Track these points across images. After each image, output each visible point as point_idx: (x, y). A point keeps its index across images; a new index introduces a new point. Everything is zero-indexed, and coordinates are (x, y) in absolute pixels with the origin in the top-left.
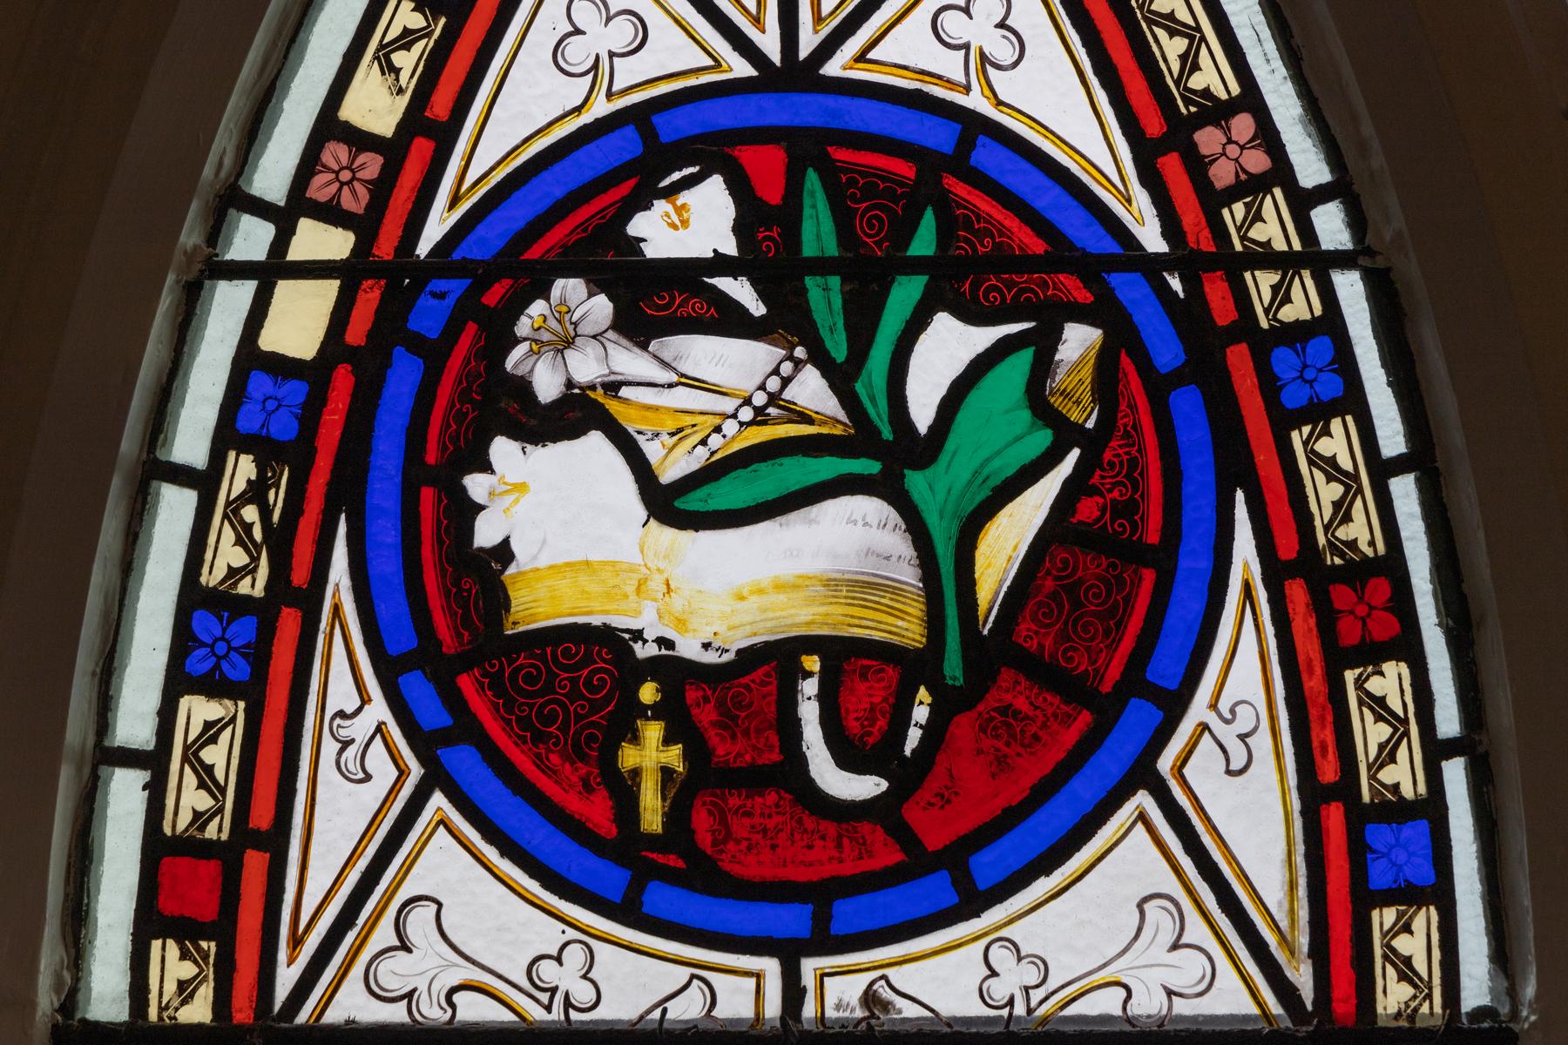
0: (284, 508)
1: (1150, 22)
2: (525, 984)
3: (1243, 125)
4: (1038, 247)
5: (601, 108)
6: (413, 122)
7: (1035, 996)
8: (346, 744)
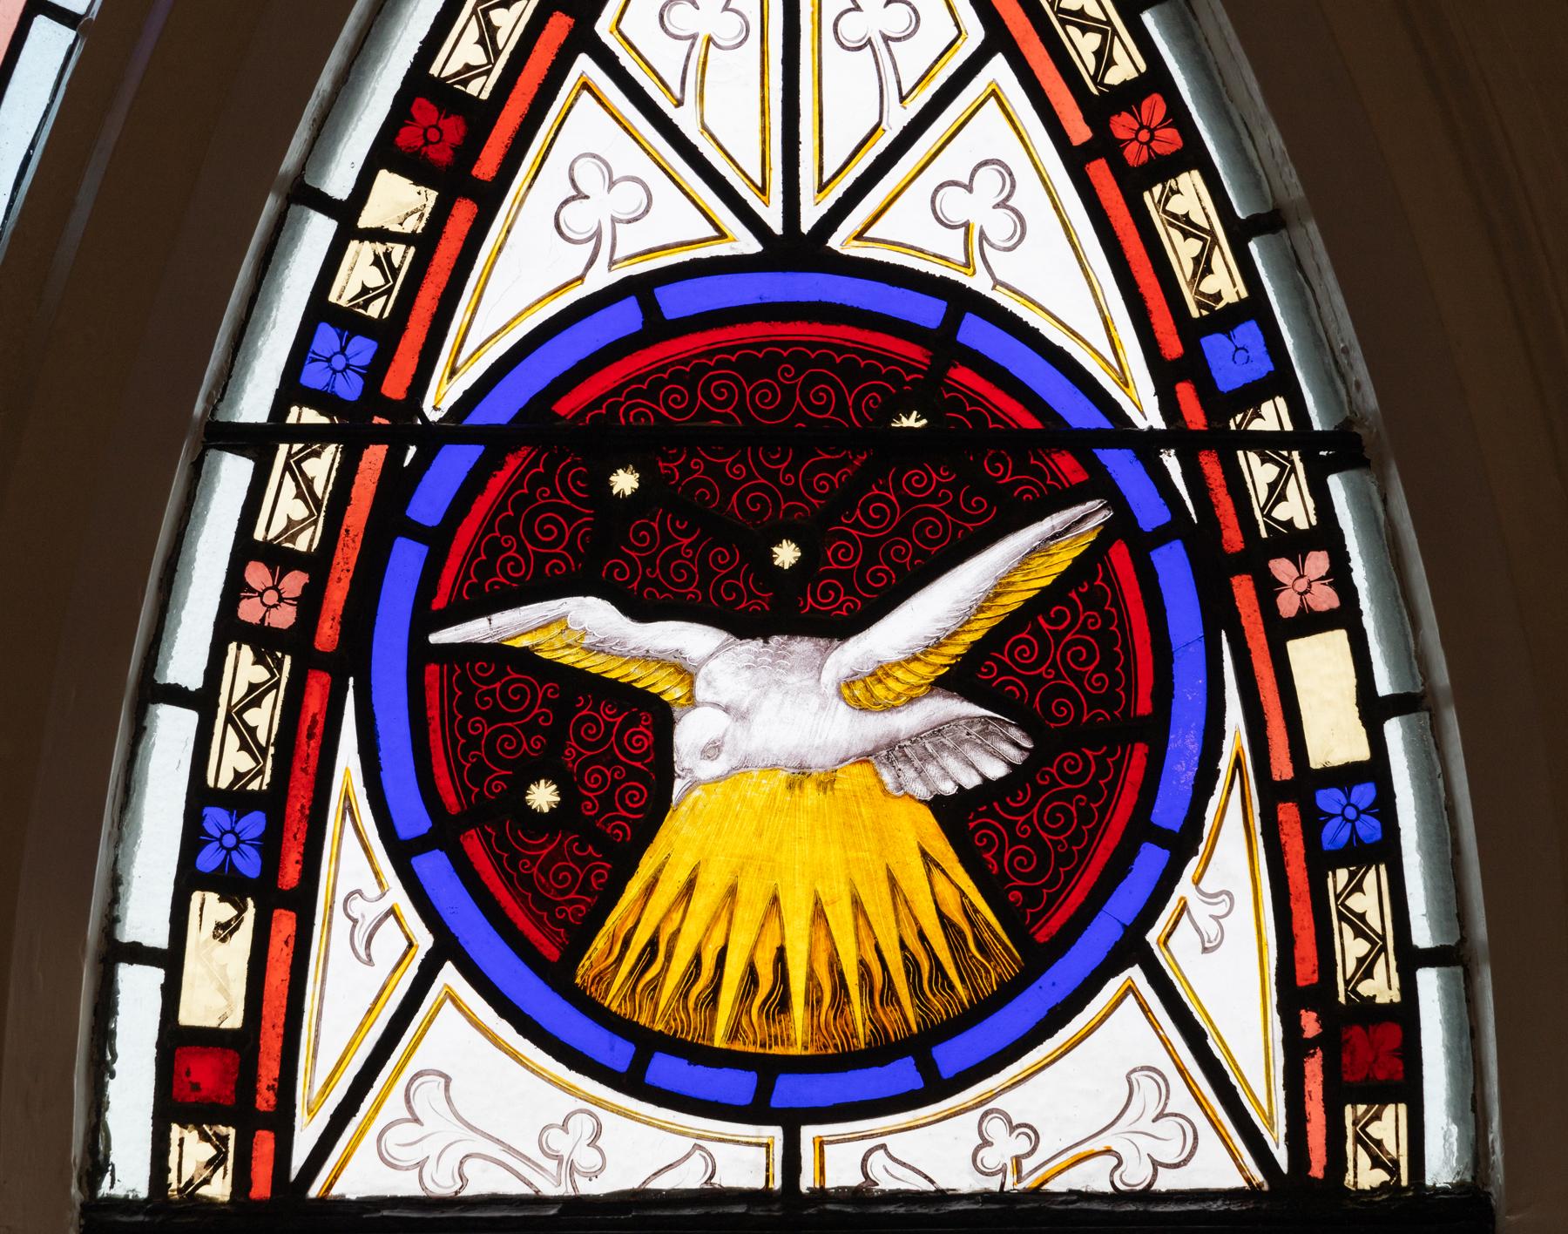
0: (291, 673)
1: (1342, 917)
2: (534, 1152)
3: (1318, 563)
4: (1030, 422)
5: (600, 279)
7: (1027, 1165)
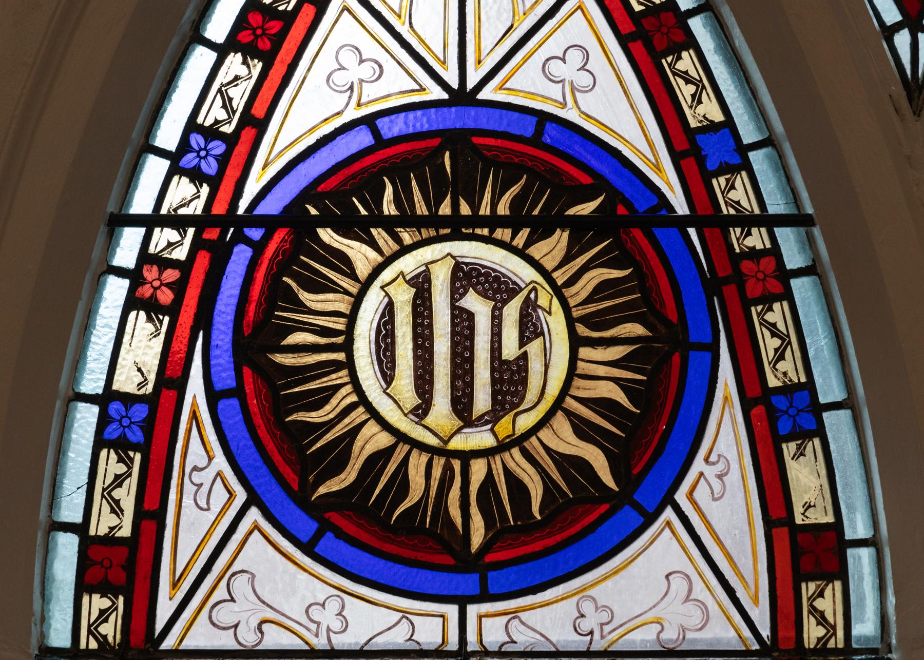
1: (674, 74)
5: (352, 114)
8: (200, 486)
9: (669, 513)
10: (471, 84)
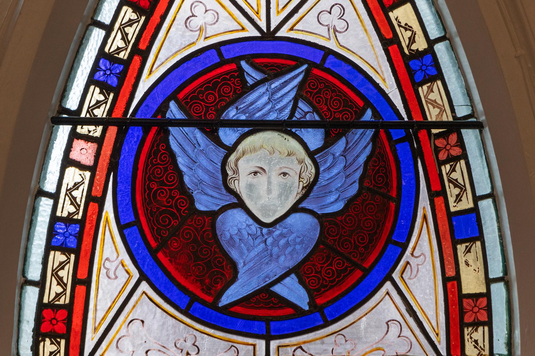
6: (135, 51)
9: (388, 285)
10: (273, 27)
